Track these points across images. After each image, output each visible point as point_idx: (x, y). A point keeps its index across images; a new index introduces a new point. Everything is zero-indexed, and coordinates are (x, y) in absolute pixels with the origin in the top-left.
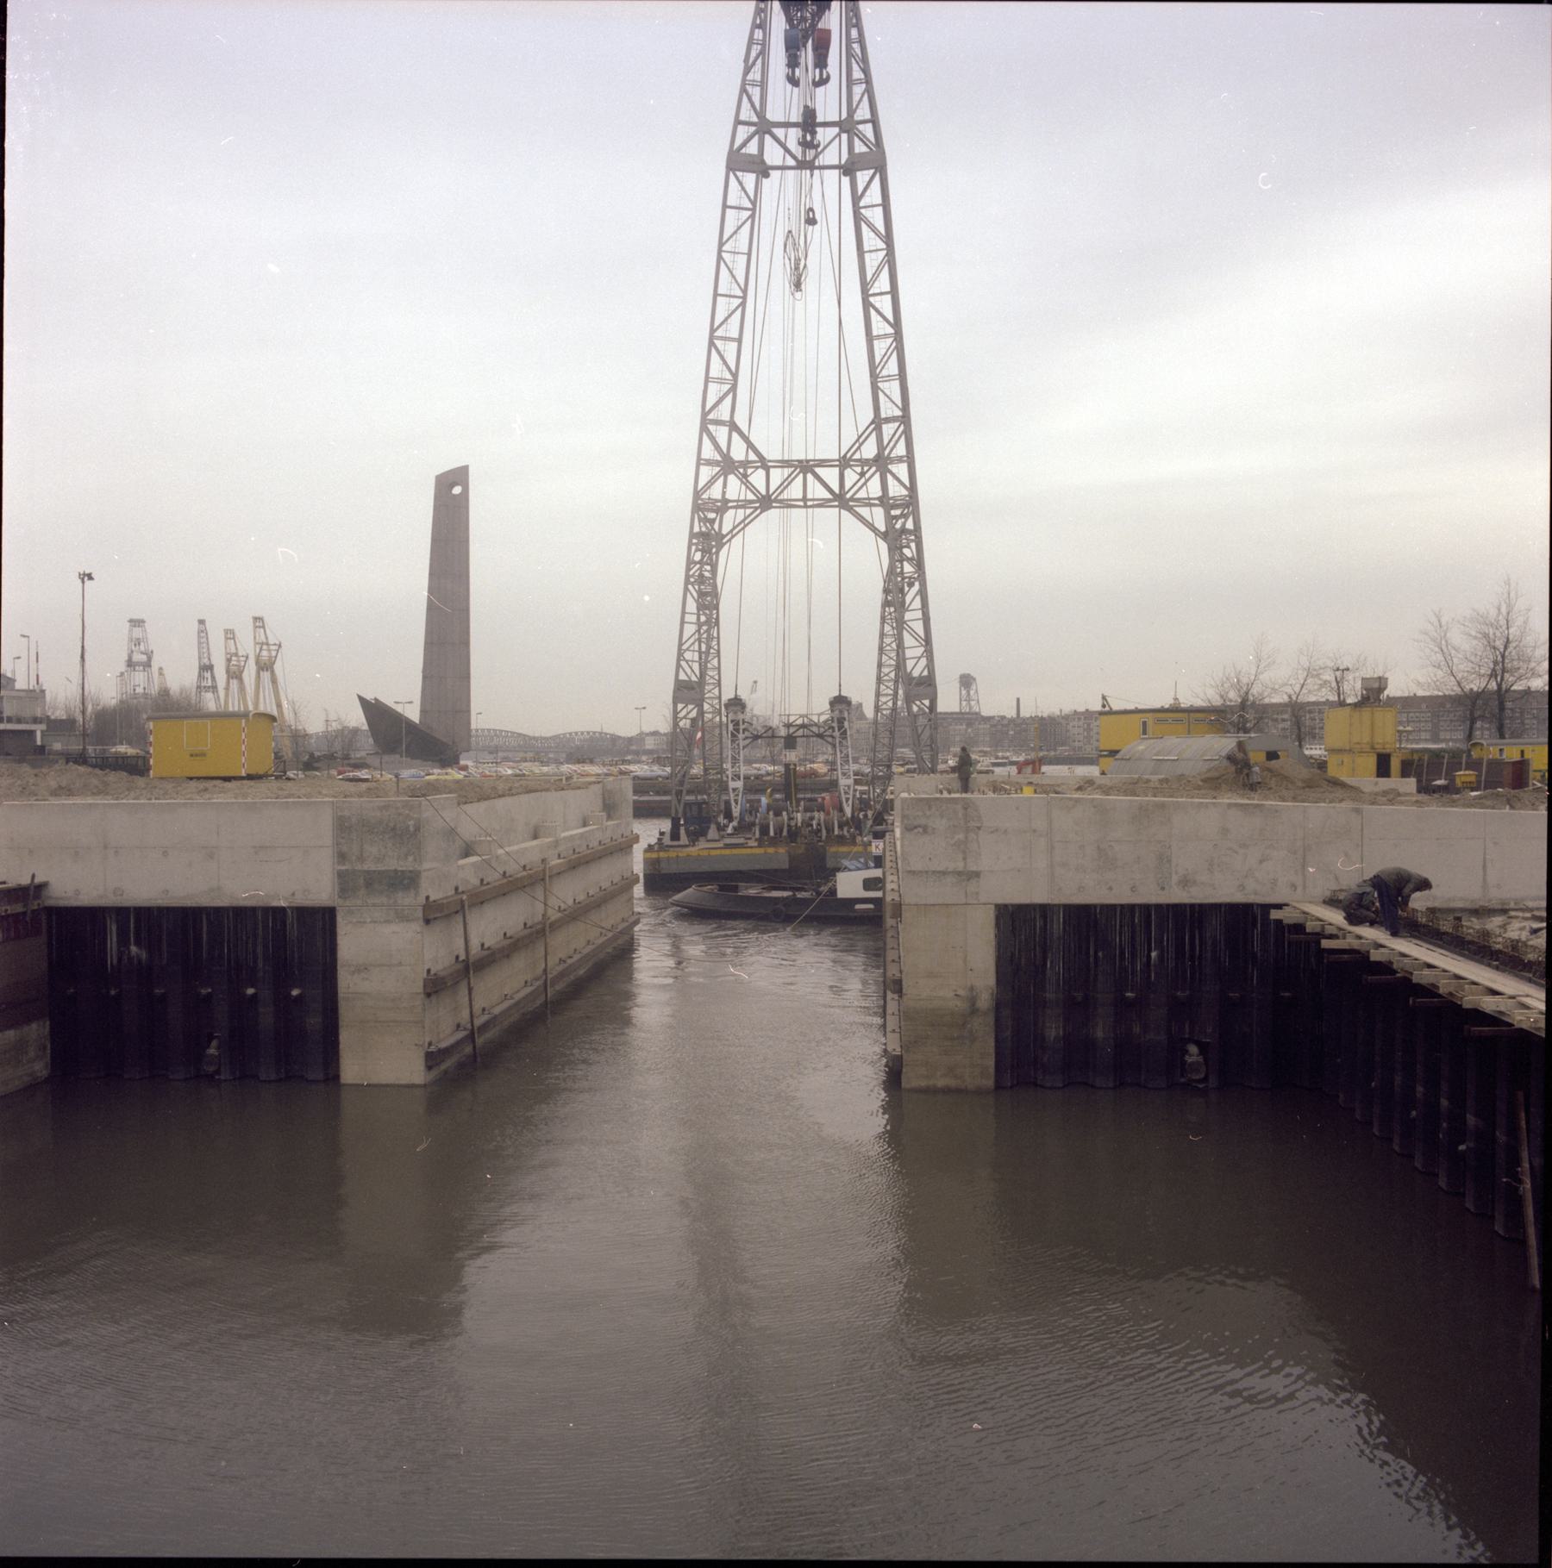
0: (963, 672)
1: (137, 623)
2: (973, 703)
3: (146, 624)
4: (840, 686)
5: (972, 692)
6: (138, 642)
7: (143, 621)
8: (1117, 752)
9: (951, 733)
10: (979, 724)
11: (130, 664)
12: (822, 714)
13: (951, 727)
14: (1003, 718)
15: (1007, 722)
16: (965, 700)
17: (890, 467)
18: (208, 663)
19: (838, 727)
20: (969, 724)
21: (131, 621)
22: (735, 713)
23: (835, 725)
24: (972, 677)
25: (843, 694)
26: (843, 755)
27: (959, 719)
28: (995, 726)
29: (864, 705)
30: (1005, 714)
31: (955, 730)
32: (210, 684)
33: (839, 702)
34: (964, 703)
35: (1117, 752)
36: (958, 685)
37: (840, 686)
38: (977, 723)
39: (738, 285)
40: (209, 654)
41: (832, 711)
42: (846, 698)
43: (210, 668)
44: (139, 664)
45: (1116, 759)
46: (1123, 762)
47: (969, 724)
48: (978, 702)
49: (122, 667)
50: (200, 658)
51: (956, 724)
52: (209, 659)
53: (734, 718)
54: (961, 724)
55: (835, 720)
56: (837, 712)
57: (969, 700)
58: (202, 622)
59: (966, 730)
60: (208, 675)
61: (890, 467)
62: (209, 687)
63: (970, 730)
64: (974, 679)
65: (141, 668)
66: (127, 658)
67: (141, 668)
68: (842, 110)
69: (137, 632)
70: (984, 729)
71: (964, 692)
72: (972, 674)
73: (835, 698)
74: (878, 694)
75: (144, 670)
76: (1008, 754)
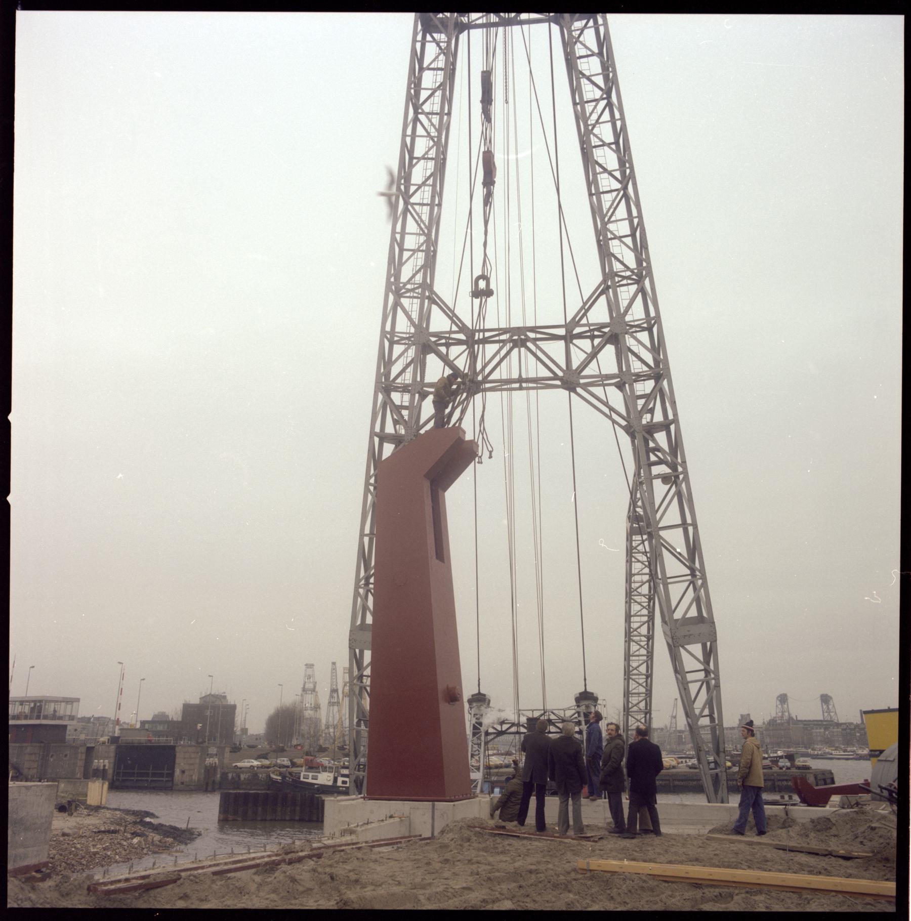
0: (822, 693)
1: (310, 666)
2: (832, 714)
3: (315, 667)
4: (585, 680)
5: (830, 707)
6: (309, 677)
7: (313, 665)
8: (881, 752)
9: (815, 734)
10: (833, 728)
11: (304, 690)
12: (569, 709)
13: (813, 731)
14: (851, 724)
15: (853, 727)
16: (827, 712)
17: (413, 330)
18: (335, 688)
19: (585, 720)
20: (826, 729)
21: (306, 665)
22: (479, 707)
23: (582, 719)
24: (829, 696)
25: (588, 690)
26: (477, 758)
27: (819, 725)
28: (845, 729)
29: (742, 713)
30: (852, 721)
31: (816, 732)
32: (336, 701)
33: (586, 697)
34: (826, 714)
35: (881, 752)
36: (820, 702)
37: (585, 680)
38: (831, 727)
39: (510, 362)
40: (337, 683)
41: (578, 706)
42: (592, 694)
43: (336, 691)
44: (309, 690)
45: (879, 760)
46: (887, 764)
47: (826, 729)
48: (836, 713)
49: (300, 692)
50: (331, 685)
51: (817, 729)
52: (336, 686)
53: (477, 712)
54: (821, 729)
55: (582, 714)
56: (583, 708)
57: (829, 712)
58: (334, 664)
59: (824, 732)
60: (335, 695)
61: (413, 330)
62: (335, 703)
63: (827, 733)
64: (831, 698)
65: (310, 692)
66: (302, 686)
67: (310, 692)
68: (514, 139)
69: (309, 671)
70: (837, 731)
71: (825, 707)
72: (829, 694)
73: (580, 694)
74: (627, 694)
75: (312, 694)
76: (855, 748)
